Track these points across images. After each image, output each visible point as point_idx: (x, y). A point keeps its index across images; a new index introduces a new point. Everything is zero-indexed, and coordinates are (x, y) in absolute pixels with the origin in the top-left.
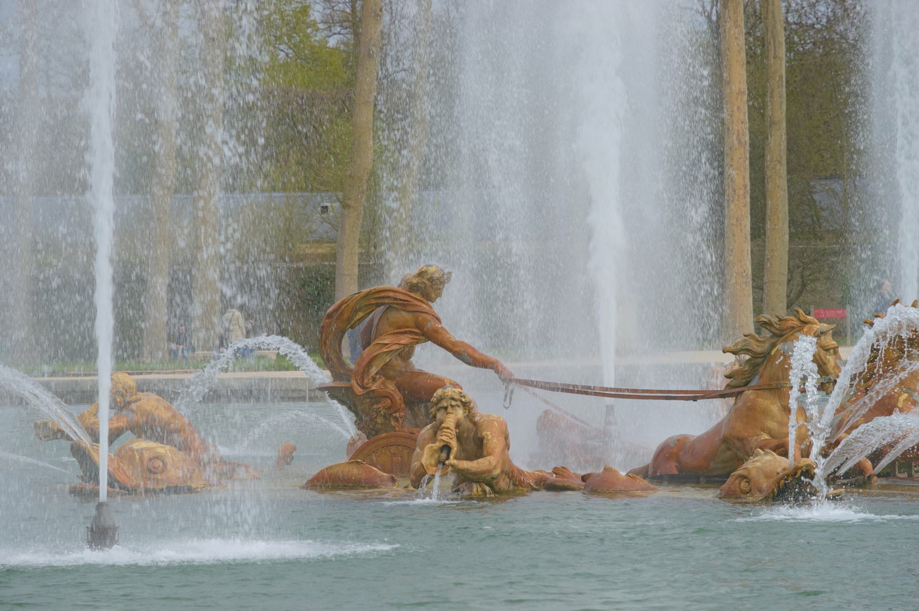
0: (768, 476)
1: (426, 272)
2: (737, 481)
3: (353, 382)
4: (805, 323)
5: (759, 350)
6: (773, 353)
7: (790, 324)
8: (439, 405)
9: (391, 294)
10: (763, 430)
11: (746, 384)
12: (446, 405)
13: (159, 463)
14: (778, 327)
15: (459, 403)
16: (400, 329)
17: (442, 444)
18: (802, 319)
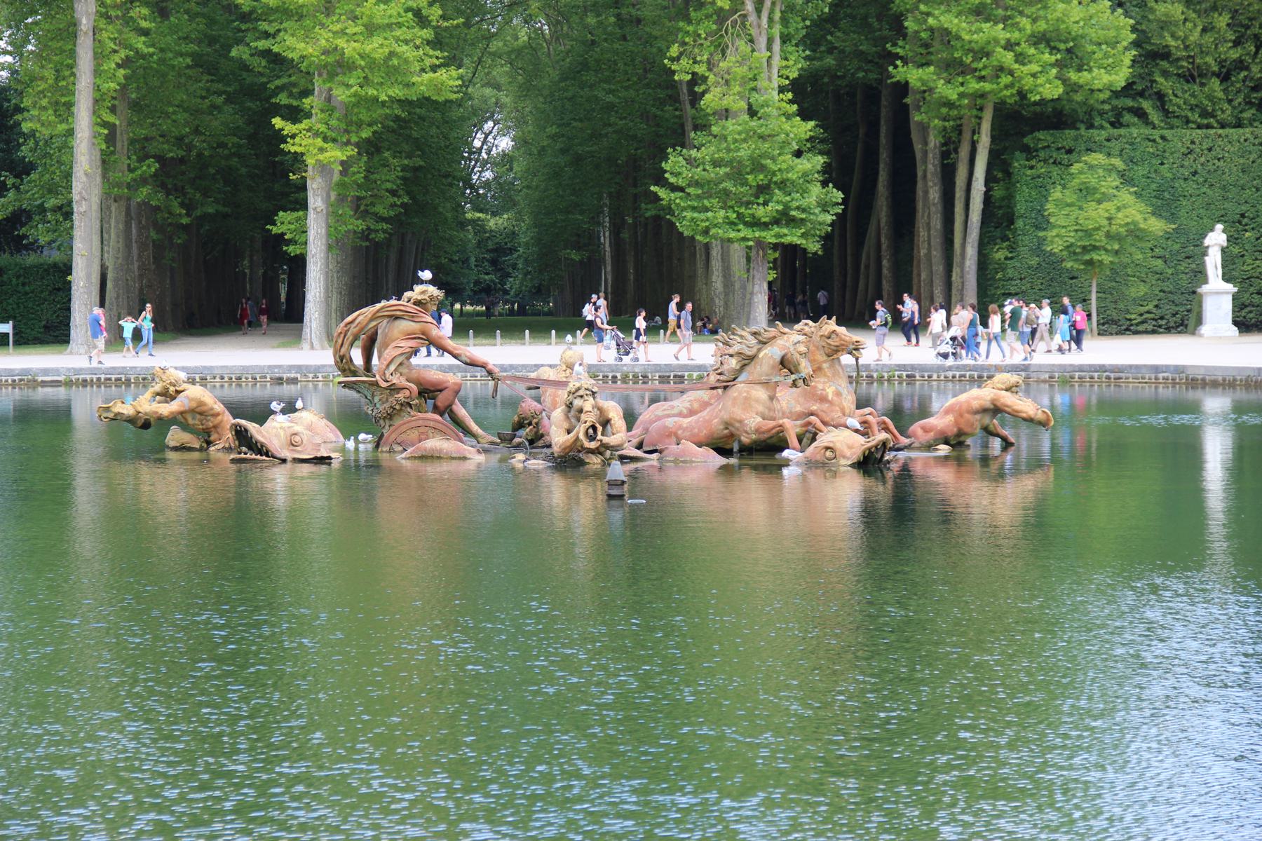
0: (850, 447)
5: (750, 353)
6: (761, 355)
13: (297, 438)
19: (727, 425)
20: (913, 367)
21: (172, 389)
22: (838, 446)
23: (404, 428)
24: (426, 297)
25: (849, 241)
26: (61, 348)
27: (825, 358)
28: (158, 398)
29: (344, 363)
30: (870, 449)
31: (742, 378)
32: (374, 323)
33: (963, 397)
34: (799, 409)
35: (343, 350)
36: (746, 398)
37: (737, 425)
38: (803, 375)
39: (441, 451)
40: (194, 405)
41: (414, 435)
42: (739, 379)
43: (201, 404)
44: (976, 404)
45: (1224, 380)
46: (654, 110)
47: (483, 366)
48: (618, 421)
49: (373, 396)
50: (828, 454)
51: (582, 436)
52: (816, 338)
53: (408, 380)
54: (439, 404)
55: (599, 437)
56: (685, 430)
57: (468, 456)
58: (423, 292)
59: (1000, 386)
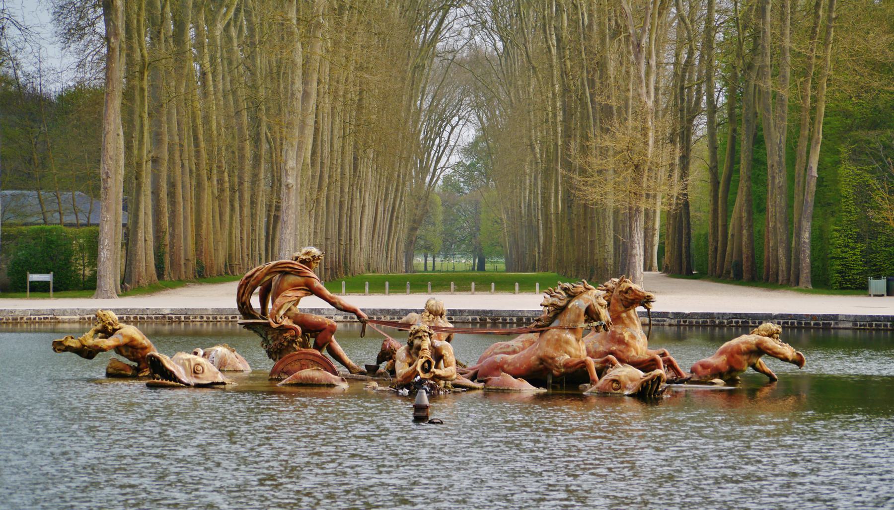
0: (632, 380)
6: (569, 306)
11: (548, 326)
19: (542, 360)
20: (485, 312)
21: (110, 327)
22: (623, 379)
25: (720, 215)
26: (90, 292)
27: (623, 309)
28: (100, 334)
29: (244, 307)
30: (647, 381)
31: (554, 324)
32: (268, 278)
33: (735, 342)
34: (602, 349)
35: (244, 298)
36: (557, 340)
37: (550, 361)
38: (604, 323)
39: (313, 379)
40: (127, 340)
41: (297, 366)
42: (553, 325)
43: (133, 339)
44: (743, 347)
46: (788, 70)
47: (354, 311)
48: (401, 352)
49: (267, 335)
50: (615, 385)
51: (419, 369)
52: (615, 293)
53: (294, 323)
54: (319, 341)
55: (433, 369)
56: (509, 364)
57: (335, 383)
58: (307, 253)
59: (763, 333)
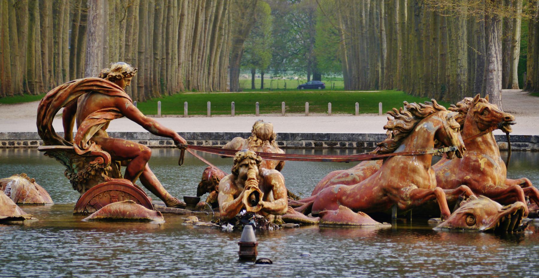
0: (489, 214)
1: (121, 68)
2: (464, 217)
3: (75, 146)
4: (439, 110)
6: (417, 130)
7: (429, 110)
8: (243, 163)
9: (99, 83)
10: (413, 182)
12: (247, 163)
14: (420, 112)
15: (255, 162)
16: (103, 108)
17: (254, 190)
18: (437, 107)
22: (478, 212)
23: (97, 192)
24: (120, 74)
32: (73, 97)
34: (454, 178)
35: (45, 121)
36: (403, 168)
37: (395, 192)
38: (456, 148)
41: (105, 199)
42: (398, 151)
45: (446, 181)
47: (171, 136)
49: (71, 163)
51: (245, 201)
52: (469, 114)
54: (130, 170)
55: (261, 202)
56: (348, 196)
57: (149, 217)
